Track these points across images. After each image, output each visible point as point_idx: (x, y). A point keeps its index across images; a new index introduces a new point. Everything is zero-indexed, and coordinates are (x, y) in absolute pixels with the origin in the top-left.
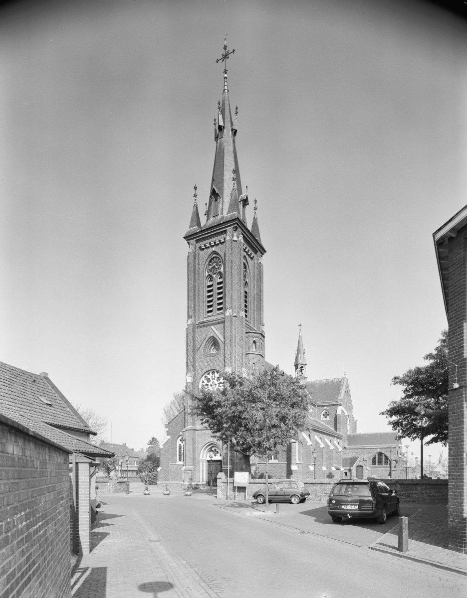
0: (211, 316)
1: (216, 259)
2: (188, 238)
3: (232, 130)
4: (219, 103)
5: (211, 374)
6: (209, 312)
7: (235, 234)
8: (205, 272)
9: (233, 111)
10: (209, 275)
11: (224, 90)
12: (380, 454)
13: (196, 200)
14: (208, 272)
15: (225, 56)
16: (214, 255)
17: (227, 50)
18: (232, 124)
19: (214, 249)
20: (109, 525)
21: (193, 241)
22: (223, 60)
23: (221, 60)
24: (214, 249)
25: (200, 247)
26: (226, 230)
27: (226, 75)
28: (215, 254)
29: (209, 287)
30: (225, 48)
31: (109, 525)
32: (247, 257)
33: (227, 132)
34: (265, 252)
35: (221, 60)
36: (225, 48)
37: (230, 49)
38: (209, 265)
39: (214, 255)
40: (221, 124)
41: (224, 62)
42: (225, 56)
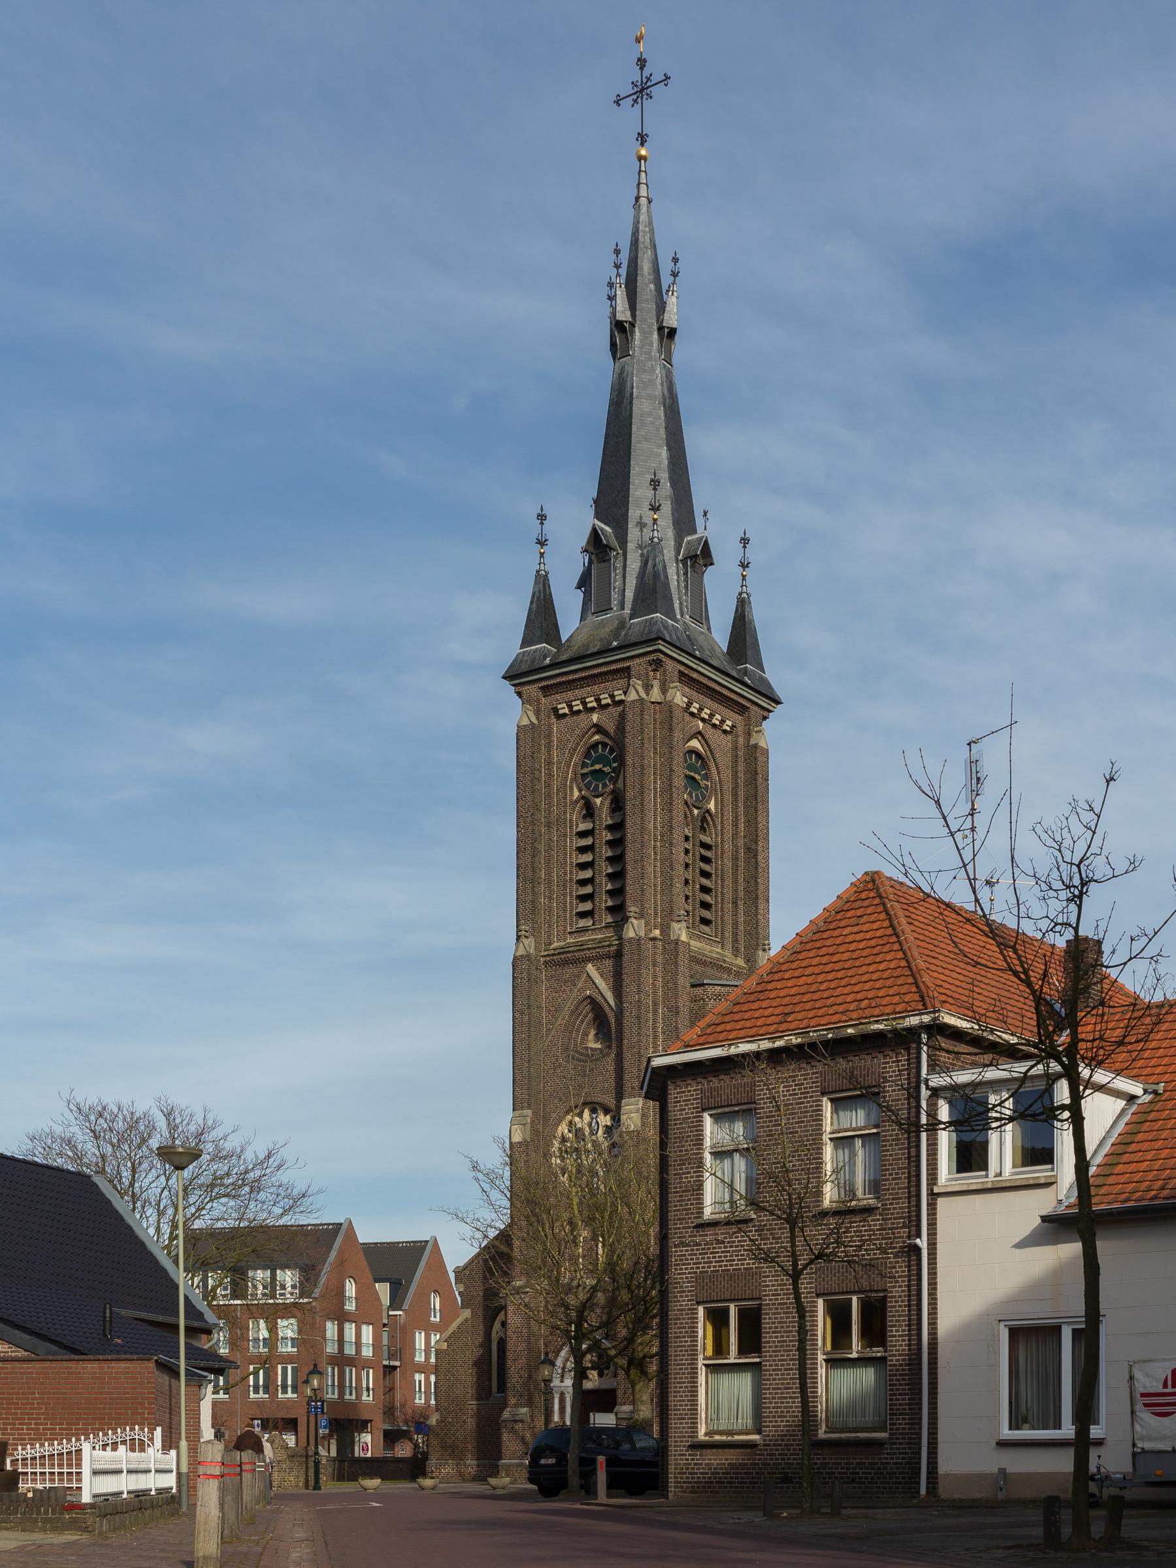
0: (584, 930)
1: (604, 750)
2: (516, 675)
3: (661, 329)
4: (617, 252)
5: (586, 1114)
6: (583, 915)
7: (656, 683)
8: (571, 789)
9: (666, 267)
10: (583, 797)
11: (637, 198)
12: (142, 1450)
13: (542, 555)
14: (580, 790)
15: (642, 91)
16: (597, 737)
17: (646, 73)
18: (661, 307)
19: (595, 717)
20: (743, 604)
21: (532, 690)
22: (635, 101)
23: (630, 100)
24: (595, 717)
25: (555, 710)
26: (629, 668)
27: (643, 152)
28: (598, 732)
29: (582, 834)
30: (642, 63)
31: (743, 604)
32: (709, 732)
33: (644, 339)
34: (778, 702)
35: (630, 100)
36: (642, 63)
37: (655, 70)
38: (584, 765)
39: (597, 737)
40: (623, 315)
41: (638, 107)
42: (642, 91)
